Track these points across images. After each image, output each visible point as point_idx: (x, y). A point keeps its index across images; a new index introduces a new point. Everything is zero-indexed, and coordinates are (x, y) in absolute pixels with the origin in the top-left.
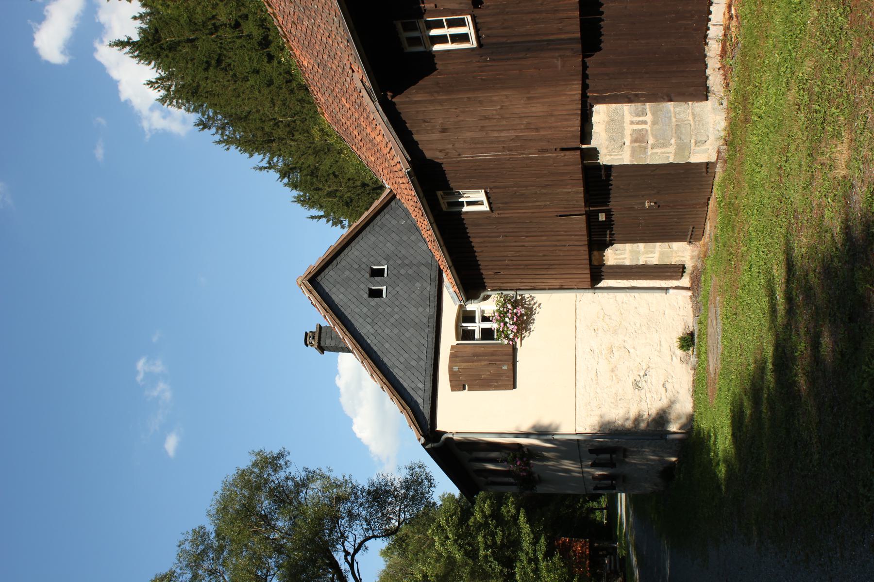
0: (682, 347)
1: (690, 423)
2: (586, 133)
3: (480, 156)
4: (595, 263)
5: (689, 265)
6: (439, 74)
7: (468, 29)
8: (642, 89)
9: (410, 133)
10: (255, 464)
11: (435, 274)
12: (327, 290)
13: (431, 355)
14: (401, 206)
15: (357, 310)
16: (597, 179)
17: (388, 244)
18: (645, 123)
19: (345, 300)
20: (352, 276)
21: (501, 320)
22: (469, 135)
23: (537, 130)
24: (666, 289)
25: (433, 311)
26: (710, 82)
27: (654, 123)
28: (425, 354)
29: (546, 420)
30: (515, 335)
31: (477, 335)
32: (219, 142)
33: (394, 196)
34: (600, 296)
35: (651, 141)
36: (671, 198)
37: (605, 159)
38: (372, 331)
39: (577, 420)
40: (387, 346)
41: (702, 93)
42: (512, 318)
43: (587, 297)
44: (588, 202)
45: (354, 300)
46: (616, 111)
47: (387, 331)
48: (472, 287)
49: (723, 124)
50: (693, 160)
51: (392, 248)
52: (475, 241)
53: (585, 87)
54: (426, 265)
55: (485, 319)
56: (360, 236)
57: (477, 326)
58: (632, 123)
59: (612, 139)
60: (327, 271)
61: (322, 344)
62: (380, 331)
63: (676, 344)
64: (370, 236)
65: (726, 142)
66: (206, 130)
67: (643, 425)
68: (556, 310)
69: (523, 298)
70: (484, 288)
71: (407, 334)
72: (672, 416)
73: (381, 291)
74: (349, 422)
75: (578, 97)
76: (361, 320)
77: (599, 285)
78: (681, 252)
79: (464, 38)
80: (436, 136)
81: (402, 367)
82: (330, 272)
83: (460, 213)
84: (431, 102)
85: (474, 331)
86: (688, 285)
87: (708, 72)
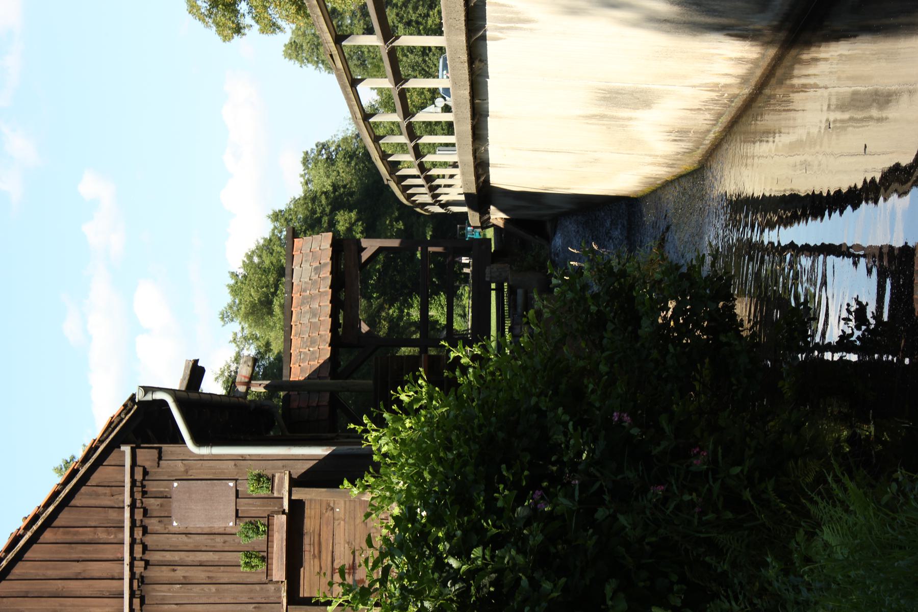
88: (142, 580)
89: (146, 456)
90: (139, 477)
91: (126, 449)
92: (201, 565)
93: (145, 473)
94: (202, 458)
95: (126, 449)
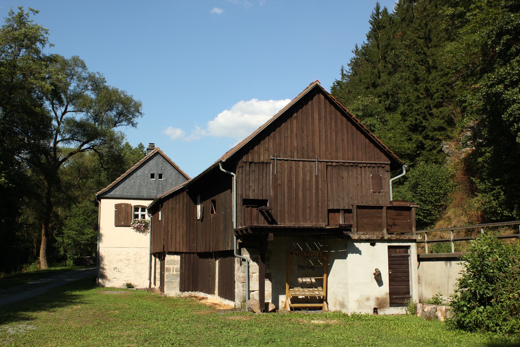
0: (127, 284)
1: (99, 285)
2: (170, 253)
9: (172, 198)
10: (135, 103)
13: (128, 197)
18: (173, 272)
22: (170, 216)
24: (150, 279)
25: (145, 197)
27: (173, 275)
28: (129, 195)
29: (104, 238)
31: (136, 213)
32: (357, 47)
34: (149, 256)
39: (104, 248)
40: (132, 181)
41: (182, 290)
43: (148, 252)
46: (178, 263)
47: (138, 181)
49: (171, 296)
51: (170, 182)
53: (186, 253)
63: (129, 282)
66: (367, 38)
67: (101, 270)
68: (143, 241)
72: (104, 280)
74: (229, 108)
75: (182, 251)
77: (153, 256)
81: (124, 186)
82: (161, 159)
87: (190, 292)
88: (357, 166)
89: (388, 168)
90: (383, 165)
91: (389, 162)
92: (362, 182)
93: (383, 167)
94: (389, 183)
95: (389, 162)
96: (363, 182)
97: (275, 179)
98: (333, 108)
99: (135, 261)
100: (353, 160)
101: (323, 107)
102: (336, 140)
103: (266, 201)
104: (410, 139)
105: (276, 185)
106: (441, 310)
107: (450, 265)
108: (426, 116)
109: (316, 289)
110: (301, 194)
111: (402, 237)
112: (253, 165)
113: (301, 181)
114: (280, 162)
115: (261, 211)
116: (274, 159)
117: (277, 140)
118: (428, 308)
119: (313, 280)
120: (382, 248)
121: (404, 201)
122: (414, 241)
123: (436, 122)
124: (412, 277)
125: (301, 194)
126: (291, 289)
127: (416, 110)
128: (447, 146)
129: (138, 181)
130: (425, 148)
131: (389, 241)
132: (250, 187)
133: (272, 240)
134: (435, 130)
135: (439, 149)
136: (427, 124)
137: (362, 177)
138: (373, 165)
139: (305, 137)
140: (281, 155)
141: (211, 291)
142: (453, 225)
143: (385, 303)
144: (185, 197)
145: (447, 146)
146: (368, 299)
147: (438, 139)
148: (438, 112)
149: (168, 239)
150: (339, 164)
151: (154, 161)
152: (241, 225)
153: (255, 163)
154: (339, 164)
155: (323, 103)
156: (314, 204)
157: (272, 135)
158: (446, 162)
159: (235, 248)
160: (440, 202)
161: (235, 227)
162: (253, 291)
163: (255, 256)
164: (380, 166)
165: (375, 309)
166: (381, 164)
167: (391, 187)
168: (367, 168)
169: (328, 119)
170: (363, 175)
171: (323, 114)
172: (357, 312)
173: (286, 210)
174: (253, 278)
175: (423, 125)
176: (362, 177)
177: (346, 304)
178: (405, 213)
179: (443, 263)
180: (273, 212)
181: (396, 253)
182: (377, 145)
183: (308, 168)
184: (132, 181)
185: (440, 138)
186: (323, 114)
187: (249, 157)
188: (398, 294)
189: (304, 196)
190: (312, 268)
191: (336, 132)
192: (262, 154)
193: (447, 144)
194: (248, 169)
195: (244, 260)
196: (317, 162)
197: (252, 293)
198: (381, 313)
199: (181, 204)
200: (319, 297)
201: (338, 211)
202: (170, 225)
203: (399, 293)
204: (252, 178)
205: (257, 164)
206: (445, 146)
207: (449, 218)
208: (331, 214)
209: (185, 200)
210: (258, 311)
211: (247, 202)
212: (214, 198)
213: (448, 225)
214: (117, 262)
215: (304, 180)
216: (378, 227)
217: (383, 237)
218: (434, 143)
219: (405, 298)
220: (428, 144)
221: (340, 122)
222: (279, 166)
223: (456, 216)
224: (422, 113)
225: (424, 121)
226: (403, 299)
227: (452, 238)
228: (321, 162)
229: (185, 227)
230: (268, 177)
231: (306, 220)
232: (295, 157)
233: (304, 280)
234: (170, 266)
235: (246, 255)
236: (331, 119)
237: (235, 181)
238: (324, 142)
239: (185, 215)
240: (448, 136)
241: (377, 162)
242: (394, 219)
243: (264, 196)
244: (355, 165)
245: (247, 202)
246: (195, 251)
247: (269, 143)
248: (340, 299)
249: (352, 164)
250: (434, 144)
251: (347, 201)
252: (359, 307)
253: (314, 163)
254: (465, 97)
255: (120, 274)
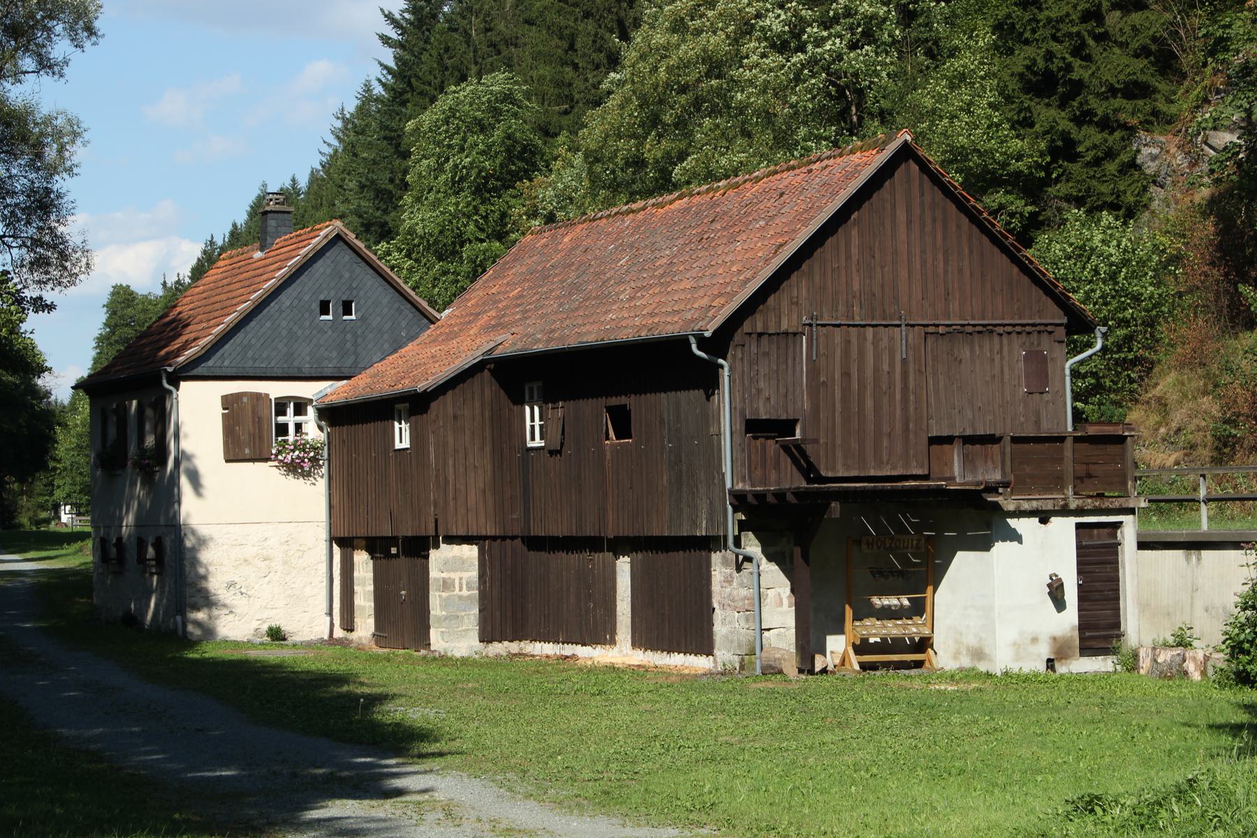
0: (271, 629)
2: (452, 540)
3: (432, 449)
4: (356, 542)
5: (354, 636)
6: (510, 410)
7: (538, 443)
8: (491, 587)
9: (454, 388)
11: (346, 373)
12: (328, 254)
14: (423, 330)
15: (306, 288)
16: (419, 547)
17: (379, 319)
18: (461, 590)
19: (317, 275)
20: (343, 281)
21: (296, 447)
22: (451, 440)
23: (455, 498)
24: (330, 614)
26: (496, 644)
27: (460, 597)
30: (281, 461)
31: (281, 419)
33: (433, 323)
34: (323, 546)
35: (444, 595)
36: (404, 615)
37: (433, 554)
38: (284, 307)
40: (268, 324)
41: (487, 636)
42: (298, 457)
43: (323, 534)
44: (405, 538)
45: (317, 285)
46: (472, 564)
48: (331, 415)
49: (458, 655)
50: (432, 631)
51: (374, 324)
52: (371, 426)
53: (494, 538)
54: (356, 362)
55: (298, 427)
56: (388, 286)
57: (290, 418)
58: (461, 579)
59: (446, 562)
60: (350, 252)
61: (269, 215)
62: (284, 315)
64: (388, 297)
65: (442, 657)
69: (321, 467)
70: (331, 425)
71: (280, 346)
73: (328, 314)
75: (484, 533)
76: (295, 294)
78: (365, 626)
79: (533, 439)
80: (450, 411)
81: (245, 342)
82: (348, 256)
83: (393, 419)
84: (482, 405)
85: (284, 414)
86: (335, 636)
87: (506, 643)
88: (991, 332)
89: (1061, 332)
90: (1049, 328)
93: (1050, 333)
95: (1065, 321)
96: (1006, 370)
97: (814, 370)
98: (939, 194)
99: (285, 563)
100: (983, 319)
101: (916, 192)
102: (946, 271)
103: (795, 422)
104: (1028, 123)
105: (816, 386)
106: (1194, 659)
107: (1199, 559)
108: (1084, 44)
109: (910, 622)
110: (869, 403)
111: (1107, 504)
112: (765, 339)
113: (869, 372)
114: (824, 330)
115: (786, 448)
116: (810, 325)
117: (817, 278)
118: (1165, 656)
119: (906, 602)
120: (1064, 529)
121: (1110, 423)
122: (1131, 511)
123: (1117, 64)
124: (1125, 590)
125: (869, 403)
126: (857, 623)
127: (1049, 20)
128: (1154, 151)
129: (284, 323)
130: (1079, 155)
131: (1079, 512)
132: (759, 391)
133: (406, 444)
134: (1113, 91)
135: (1124, 157)
136: (1086, 75)
137: (1002, 359)
138: (1028, 329)
139: (878, 269)
140: (825, 315)
141: (602, 634)
142: (1174, 425)
143: (1069, 648)
144: (486, 386)
145: (1154, 151)
146: (1035, 640)
147: (1124, 126)
148: (1127, 29)
149: (446, 502)
150: (951, 329)
151: (328, 262)
152: (743, 480)
153: (770, 335)
154: (951, 329)
155: (917, 183)
156: (898, 425)
157: (804, 267)
158: (1146, 206)
159: (732, 530)
160: (1130, 350)
161: (728, 485)
162: (769, 630)
163: (771, 550)
164: (1044, 329)
165: (1049, 660)
166: (1046, 325)
167: (1068, 379)
168: (1014, 335)
169: (928, 221)
170: (1005, 354)
171: (917, 211)
172: (1015, 668)
173: (839, 442)
174: (768, 600)
175: (1075, 76)
176: (1002, 359)
177: (987, 651)
178: (1112, 449)
179: (1179, 554)
180: (809, 449)
181: (1091, 537)
182: (1037, 279)
183: (885, 343)
184: (268, 324)
185: (1134, 121)
186: (917, 211)
187: (756, 323)
188: (1096, 627)
189: (877, 408)
190: (893, 572)
191: (946, 253)
192: (785, 314)
193: (1154, 143)
194: (754, 349)
195: (748, 559)
196: (903, 328)
197: (766, 634)
198: (1061, 669)
199: (477, 405)
200: (912, 639)
201: (949, 440)
202: (451, 462)
203: (1099, 626)
204: (763, 370)
205: (775, 338)
206: (1146, 151)
207: (1162, 405)
208: (935, 448)
209: (487, 392)
210: (791, 669)
211: (755, 427)
212: (630, 401)
213: (1159, 424)
214: (236, 567)
215: (876, 369)
216: (1056, 483)
217: (1066, 505)
218: (1111, 139)
219: (1111, 637)
220: (1088, 143)
221: (954, 229)
222: (821, 339)
223: (1185, 396)
224: (1070, 35)
225: (1077, 63)
226: (1108, 638)
227: (1202, 493)
228: (913, 326)
229: (489, 468)
230: (798, 368)
231: (882, 463)
232: (857, 318)
233: (886, 602)
234: (452, 575)
235: (752, 547)
236: (934, 220)
237: (726, 379)
238: (919, 277)
239: (488, 435)
240: (1155, 113)
241: (1038, 321)
242: (1087, 464)
243: (790, 411)
244: (988, 330)
245: (755, 427)
246: (517, 532)
247: (798, 286)
248: (971, 640)
249: (980, 329)
250: (1110, 143)
251: (970, 416)
252: (1018, 657)
253: (897, 329)
254: (1225, 27)
255: (244, 600)
